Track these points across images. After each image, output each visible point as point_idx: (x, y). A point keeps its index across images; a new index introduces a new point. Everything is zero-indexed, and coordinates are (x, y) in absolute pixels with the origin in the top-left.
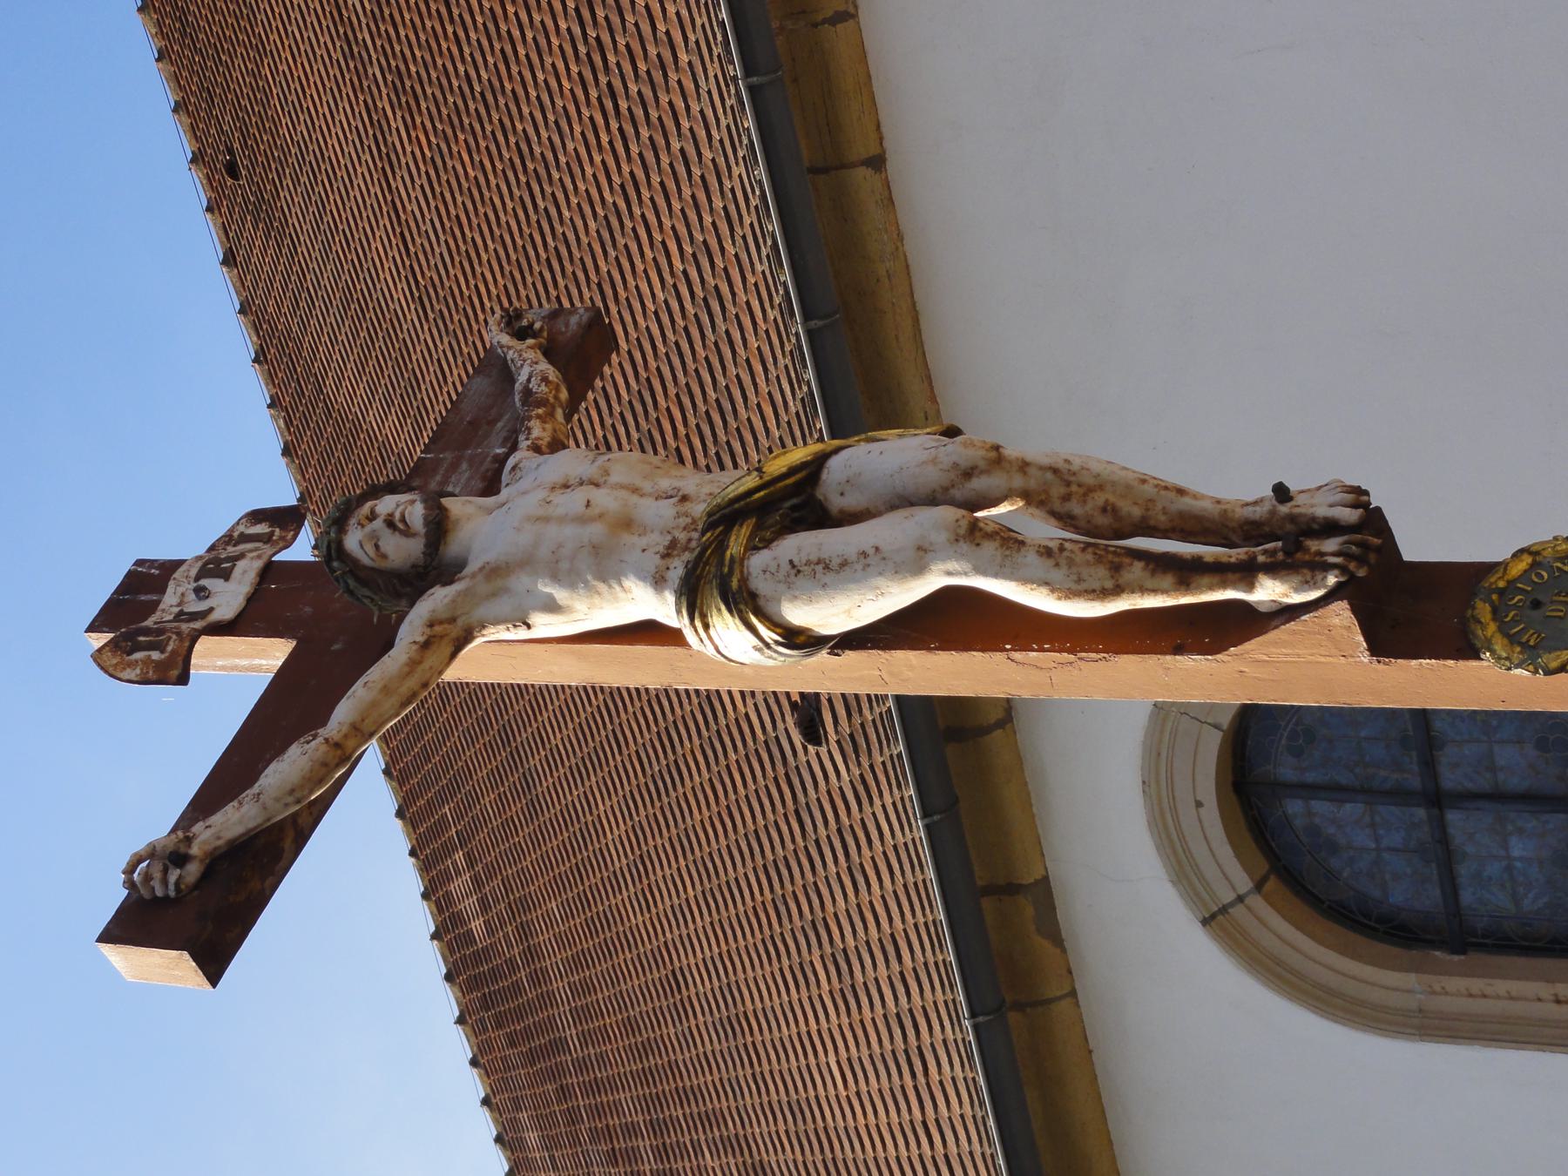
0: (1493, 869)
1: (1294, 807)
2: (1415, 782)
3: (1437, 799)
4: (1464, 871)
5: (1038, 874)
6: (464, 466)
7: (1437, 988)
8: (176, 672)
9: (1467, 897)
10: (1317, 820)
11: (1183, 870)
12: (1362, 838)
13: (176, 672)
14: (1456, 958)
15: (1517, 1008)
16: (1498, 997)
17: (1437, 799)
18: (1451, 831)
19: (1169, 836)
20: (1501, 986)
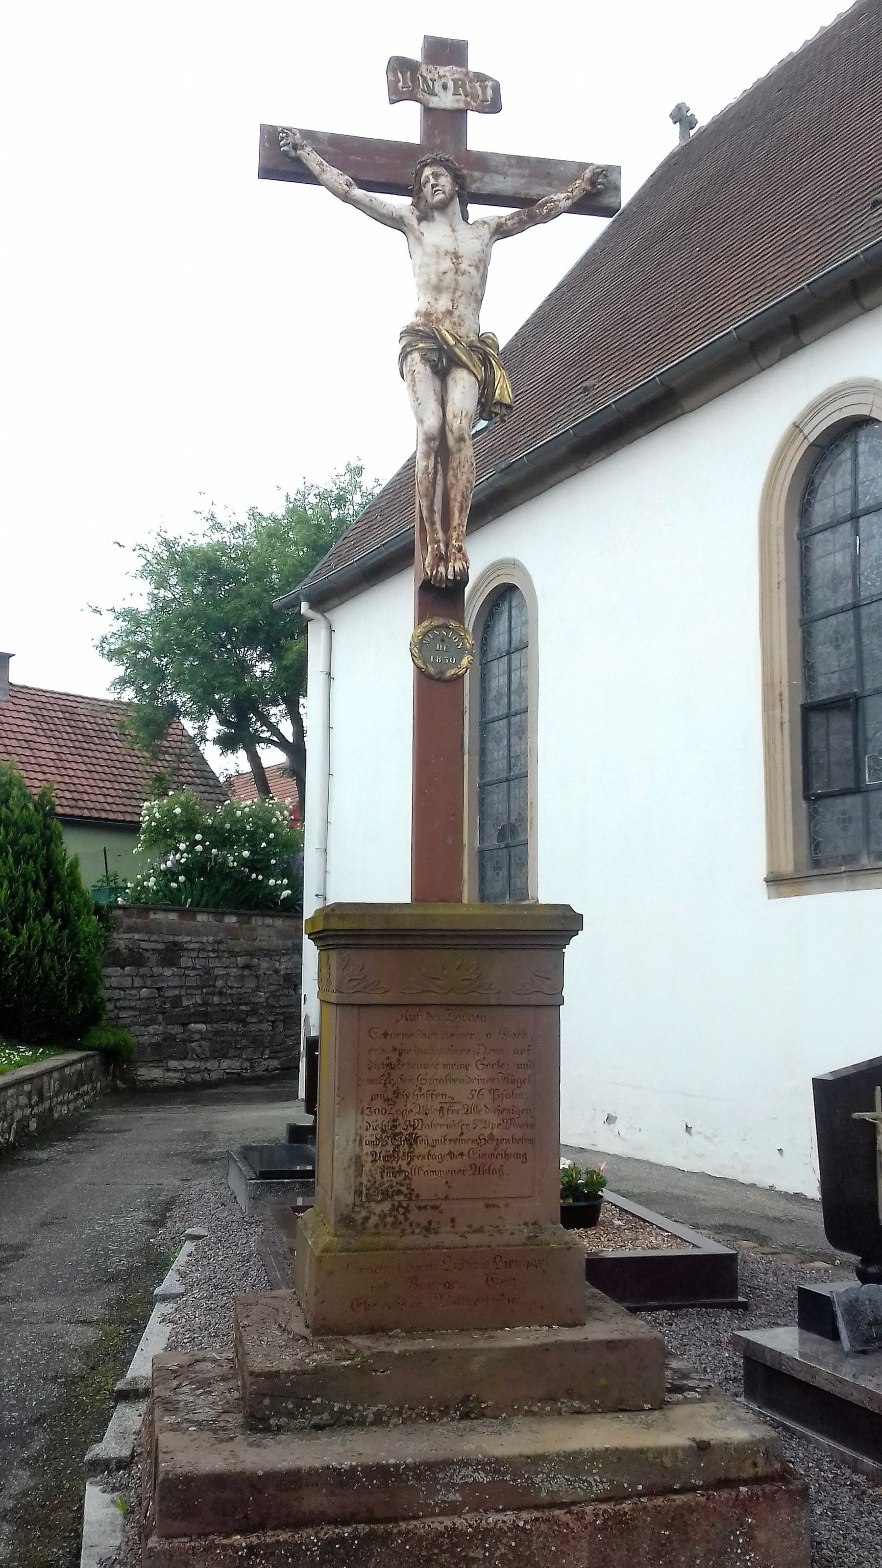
0: (830, 548)
1: (848, 454)
2: (862, 506)
3: (509, 653)
4: (828, 534)
5: (805, 342)
6: (523, 181)
7: (780, 532)
8: (396, 96)
9: (819, 537)
10: (844, 464)
11: (815, 408)
12: (839, 486)
13: (396, 96)
14: (795, 537)
15: (775, 564)
16: (778, 558)
17: (509, 653)
18: (843, 526)
19: (820, 404)
20: (782, 558)
